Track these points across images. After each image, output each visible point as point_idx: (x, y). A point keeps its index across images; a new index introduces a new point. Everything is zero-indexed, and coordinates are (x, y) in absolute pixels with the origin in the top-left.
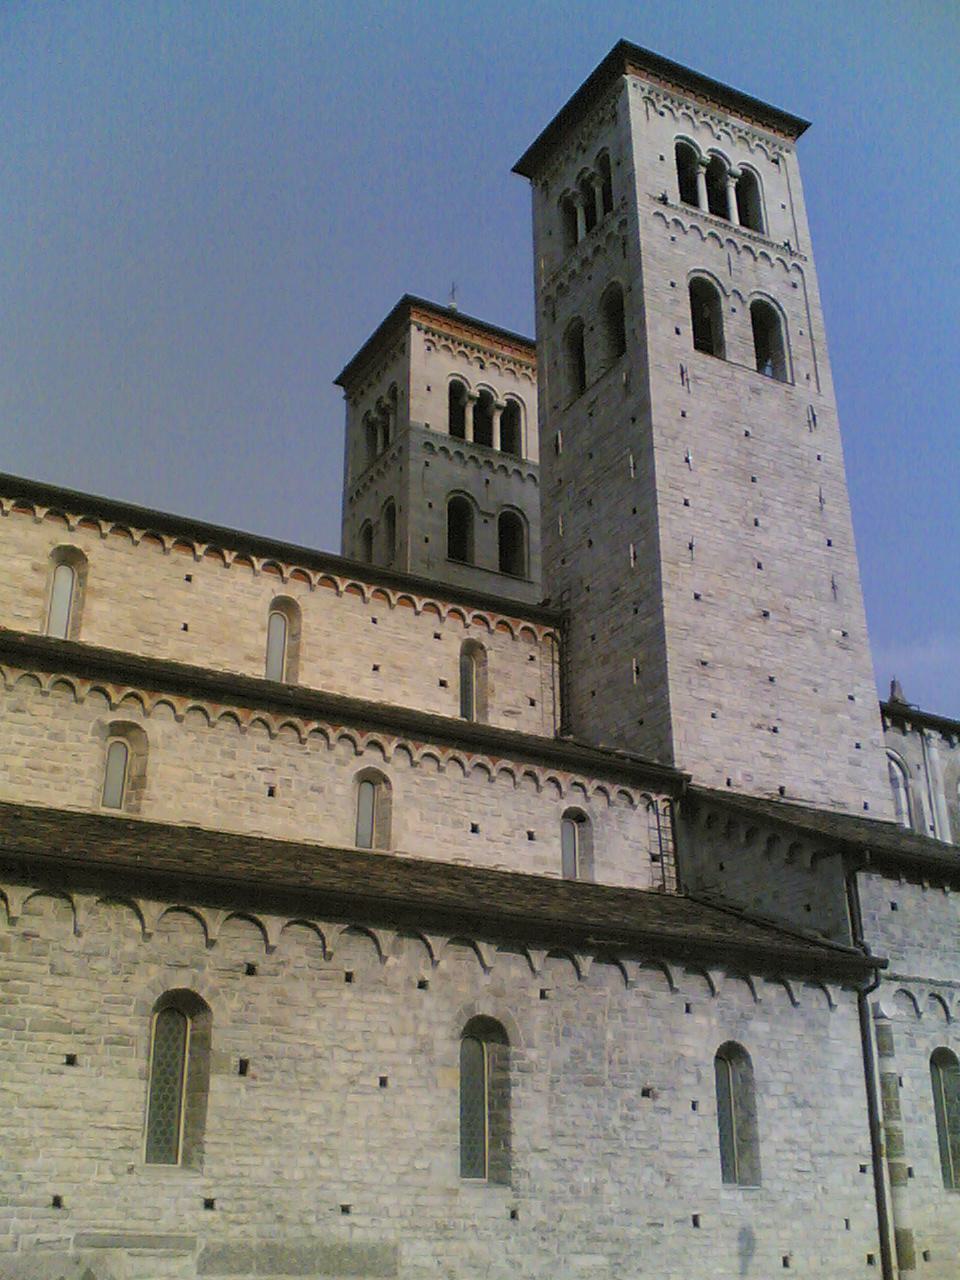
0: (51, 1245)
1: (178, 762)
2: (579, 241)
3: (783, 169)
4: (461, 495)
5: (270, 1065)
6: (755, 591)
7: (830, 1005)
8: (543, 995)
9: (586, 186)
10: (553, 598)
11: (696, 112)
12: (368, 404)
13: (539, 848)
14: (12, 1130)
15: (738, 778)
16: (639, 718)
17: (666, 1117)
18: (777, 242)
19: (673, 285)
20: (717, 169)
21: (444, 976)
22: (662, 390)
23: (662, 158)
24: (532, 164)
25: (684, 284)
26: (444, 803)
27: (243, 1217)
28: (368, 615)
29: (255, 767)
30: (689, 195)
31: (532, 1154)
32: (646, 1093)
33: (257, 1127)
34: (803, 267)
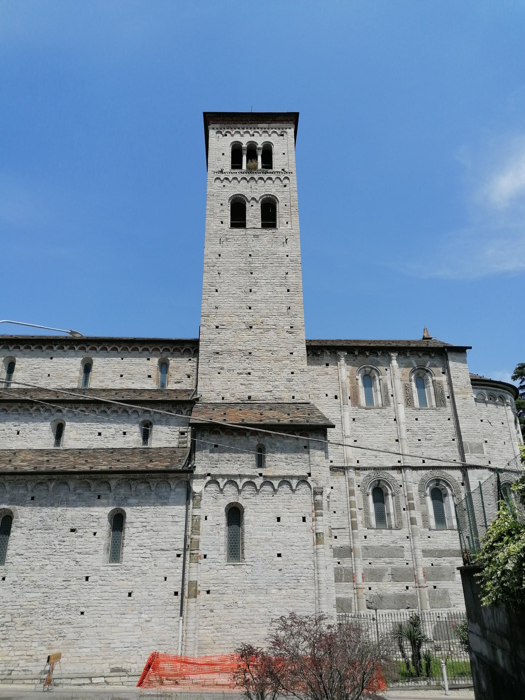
6: (246, 319)
13: (128, 438)
17: (80, 539)
26: (87, 427)
29: (12, 425)
30: (236, 163)
31: (16, 556)
32: (73, 530)
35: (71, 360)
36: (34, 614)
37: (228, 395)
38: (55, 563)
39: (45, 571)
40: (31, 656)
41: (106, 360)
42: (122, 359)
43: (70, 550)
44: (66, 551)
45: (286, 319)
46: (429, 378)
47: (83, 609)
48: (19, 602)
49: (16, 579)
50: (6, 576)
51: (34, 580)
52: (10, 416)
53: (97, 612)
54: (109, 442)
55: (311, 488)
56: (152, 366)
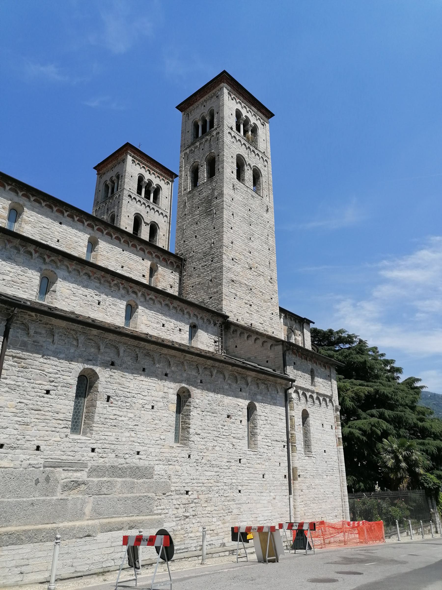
0: (34, 466)
1: (67, 288)
2: (199, 136)
3: (265, 128)
5: (117, 398)
7: (278, 392)
8: (201, 382)
12: (107, 177)
14: (23, 419)
15: (240, 318)
18: (261, 151)
19: (232, 157)
20: (246, 122)
21: (173, 372)
22: (227, 190)
23: (232, 114)
24: (182, 107)
25: (235, 157)
27: (105, 455)
29: (94, 294)
32: (228, 416)
33: (111, 421)
34: (268, 161)
35: (80, 234)
36: (212, 491)
38: (221, 445)
39: (215, 452)
40: (213, 530)
41: (110, 246)
42: (123, 251)
43: (229, 434)
44: (226, 435)
45: (269, 271)
46: (293, 336)
47: (240, 488)
48: (202, 480)
49: (198, 458)
50: (191, 453)
51: (209, 459)
52: (91, 283)
53: (248, 490)
54: (170, 335)
55: (333, 405)
56: (146, 267)
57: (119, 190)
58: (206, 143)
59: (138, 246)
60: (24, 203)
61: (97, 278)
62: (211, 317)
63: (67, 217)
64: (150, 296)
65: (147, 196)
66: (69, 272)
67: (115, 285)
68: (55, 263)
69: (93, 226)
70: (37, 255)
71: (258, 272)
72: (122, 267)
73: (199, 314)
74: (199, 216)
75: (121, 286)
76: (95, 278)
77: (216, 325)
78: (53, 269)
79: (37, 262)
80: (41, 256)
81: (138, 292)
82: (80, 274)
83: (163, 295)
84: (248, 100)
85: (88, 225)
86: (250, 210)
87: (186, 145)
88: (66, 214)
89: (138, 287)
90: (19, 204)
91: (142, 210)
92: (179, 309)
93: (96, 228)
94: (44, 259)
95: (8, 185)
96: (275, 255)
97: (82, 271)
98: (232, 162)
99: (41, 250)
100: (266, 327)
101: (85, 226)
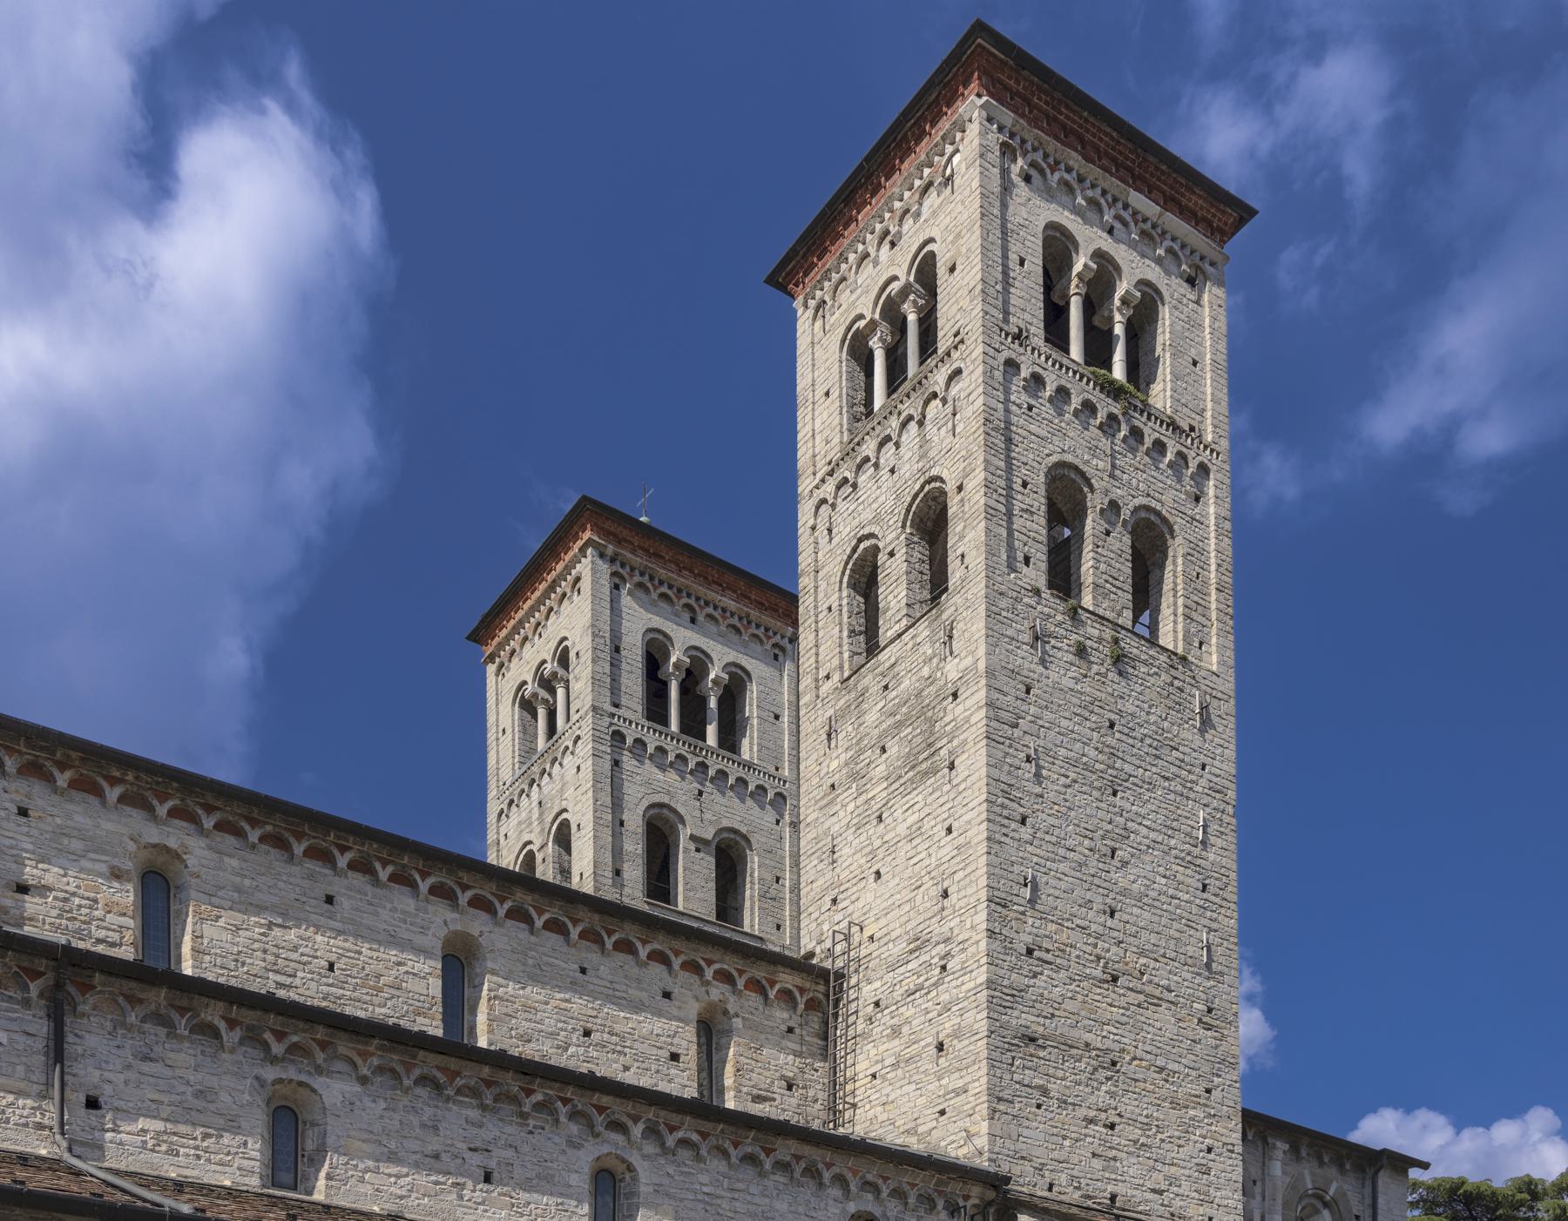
1: (365, 1136)
2: (876, 408)
4: (665, 811)
9: (892, 313)
10: (818, 950)
11: (1081, 180)
15: (1063, 1178)
16: (940, 1107)
28: (576, 963)
37: (1063, 1178)
52: (449, 1110)
57: (574, 718)
58: (904, 438)
59: (639, 945)
60: (182, 845)
61: (467, 1091)
62: (935, 1185)
63: (350, 873)
64: (680, 1134)
65: (693, 726)
66: (363, 1081)
67: (538, 1107)
68: (308, 1054)
69: (454, 892)
70: (237, 1034)
71: (1149, 989)
72: (587, 1033)
73: (885, 1179)
74: (885, 785)
75: (563, 1110)
76: (459, 1092)
77: (960, 1212)
78: (303, 1078)
79: (244, 1060)
80: (253, 1037)
81: (630, 1123)
82: (402, 1084)
83: (732, 1124)
84: (1114, 160)
85: (433, 890)
86: (1112, 726)
87: (818, 467)
88: (343, 861)
89: (629, 1107)
90: (167, 849)
91: (676, 789)
92: (798, 1170)
93: (464, 898)
94: (266, 1046)
95: (112, 785)
96: (1233, 906)
97: (408, 1071)
98: (1026, 511)
99: (250, 1016)
100: (1178, 1203)
101: (421, 897)
